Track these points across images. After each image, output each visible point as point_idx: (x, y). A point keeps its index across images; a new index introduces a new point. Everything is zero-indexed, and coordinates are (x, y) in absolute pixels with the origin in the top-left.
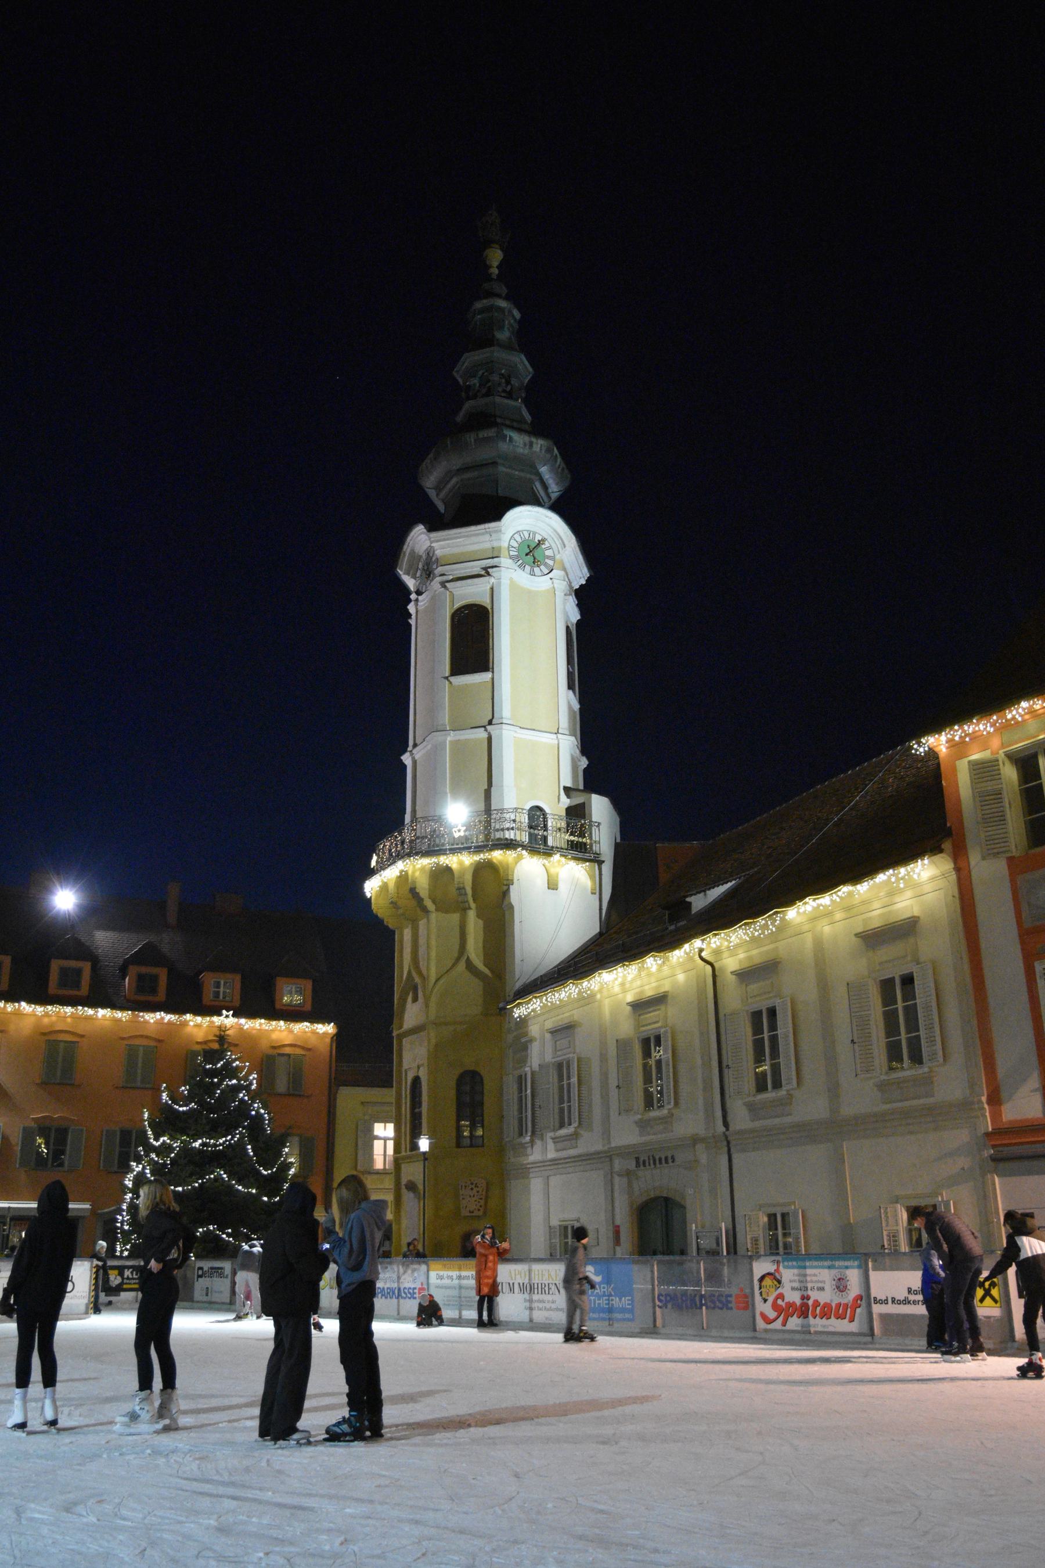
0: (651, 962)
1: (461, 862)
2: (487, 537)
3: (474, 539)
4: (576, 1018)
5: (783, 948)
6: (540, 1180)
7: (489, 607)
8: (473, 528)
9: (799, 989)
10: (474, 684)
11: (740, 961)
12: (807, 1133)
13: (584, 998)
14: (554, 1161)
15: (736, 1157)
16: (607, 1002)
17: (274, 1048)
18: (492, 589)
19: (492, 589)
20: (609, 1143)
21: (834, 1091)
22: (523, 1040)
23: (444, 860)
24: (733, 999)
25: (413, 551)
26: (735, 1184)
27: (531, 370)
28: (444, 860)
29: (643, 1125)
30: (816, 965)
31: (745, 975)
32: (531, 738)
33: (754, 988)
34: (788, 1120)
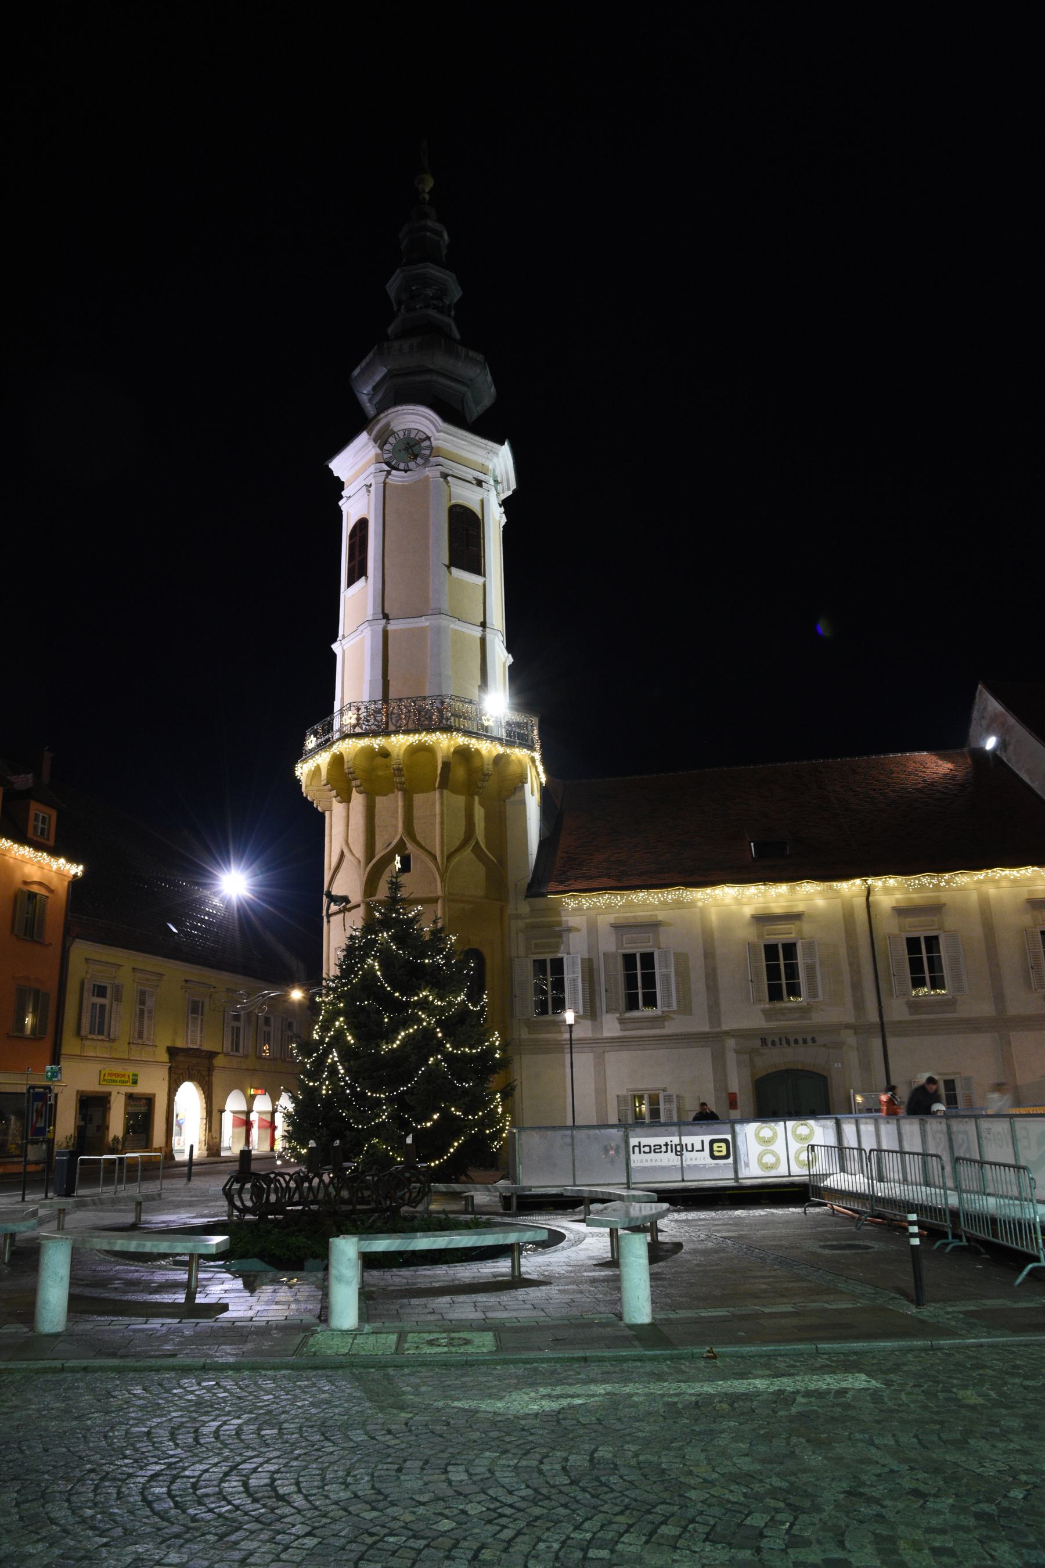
0: (783, 888)
1: (487, 749)
2: (483, 452)
3: (473, 448)
4: (660, 918)
5: (944, 897)
6: (590, 1057)
7: (480, 516)
8: (478, 439)
9: (665, 950)
10: (467, 582)
11: (897, 900)
12: (974, 1025)
13: (682, 902)
14: (612, 1040)
15: (891, 1041)
16: (713, 910)
17: (25, 883)
18: (482, 501)
19: (482, 501)
20: (719, 1025)
21: (999, 997)
22: (557, 929)
23: (474, 743)
24: (887, 926)
25: (388, 425)
26: (890, 1061)
27: (398, 271)
28: (474, 743)
29: (768, 1014)
30: (845, 919)
31: (900, 911)
32: (412, 626)
33: (909, 920)
34: (955, 1015)
